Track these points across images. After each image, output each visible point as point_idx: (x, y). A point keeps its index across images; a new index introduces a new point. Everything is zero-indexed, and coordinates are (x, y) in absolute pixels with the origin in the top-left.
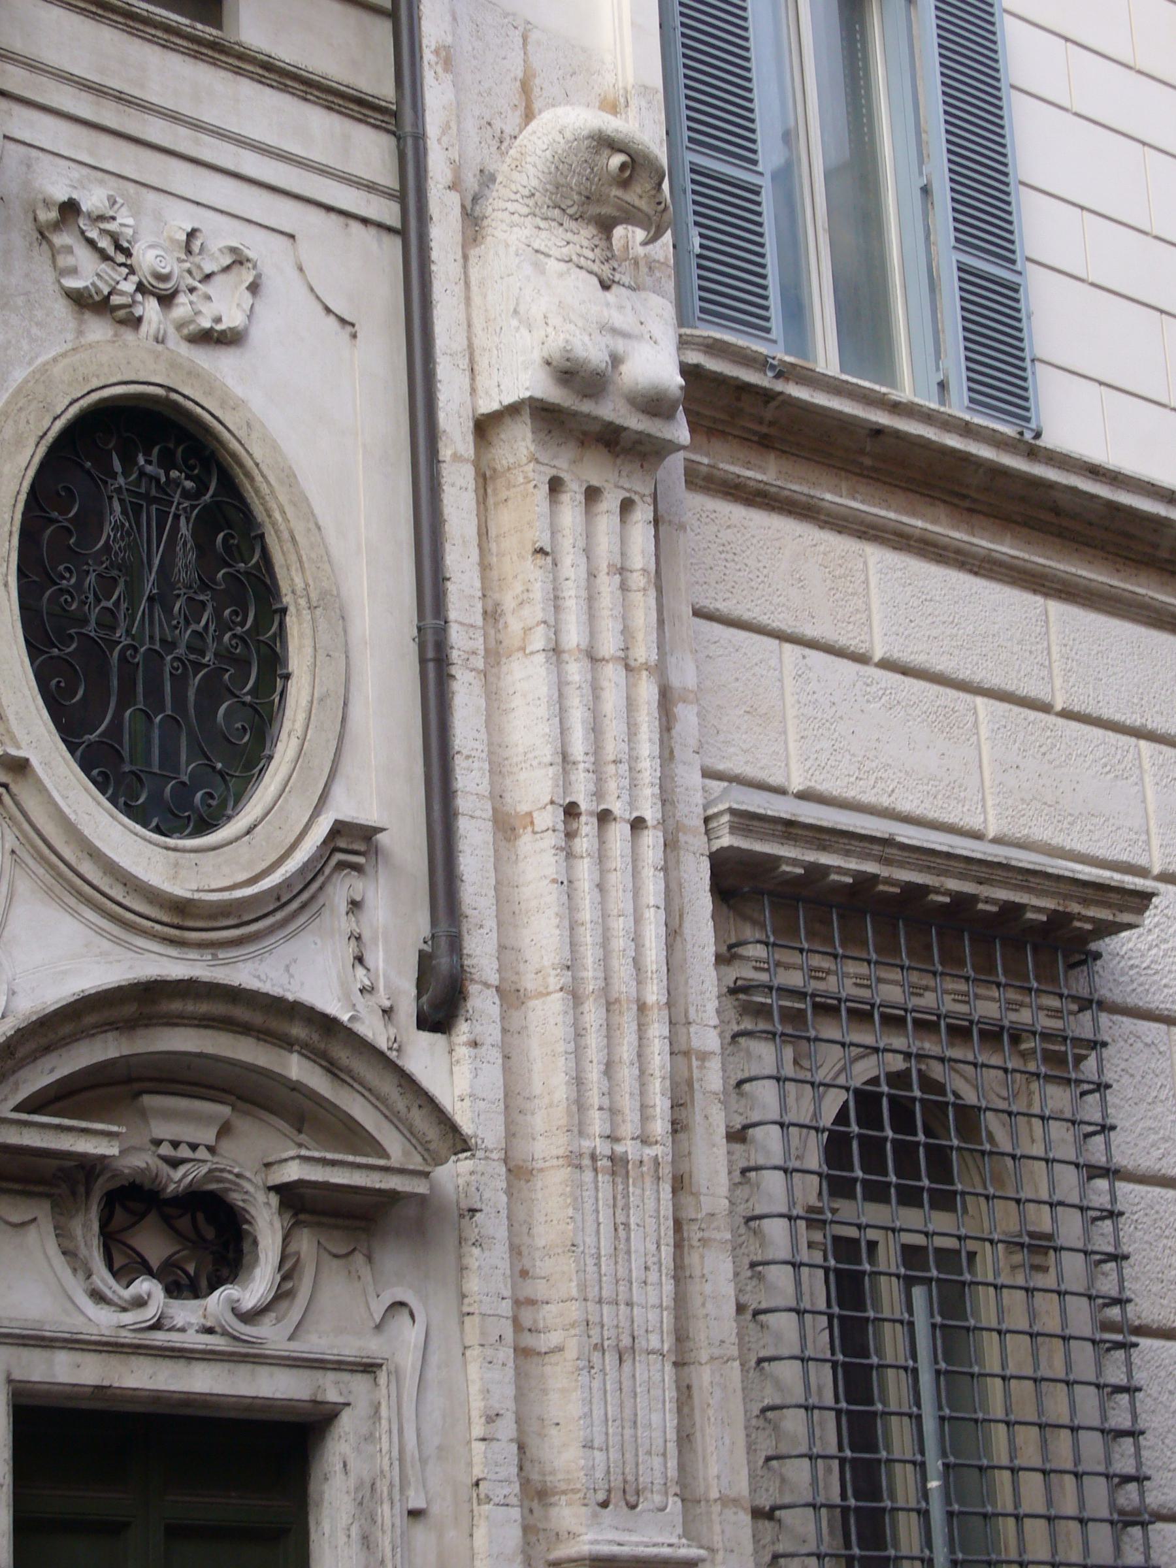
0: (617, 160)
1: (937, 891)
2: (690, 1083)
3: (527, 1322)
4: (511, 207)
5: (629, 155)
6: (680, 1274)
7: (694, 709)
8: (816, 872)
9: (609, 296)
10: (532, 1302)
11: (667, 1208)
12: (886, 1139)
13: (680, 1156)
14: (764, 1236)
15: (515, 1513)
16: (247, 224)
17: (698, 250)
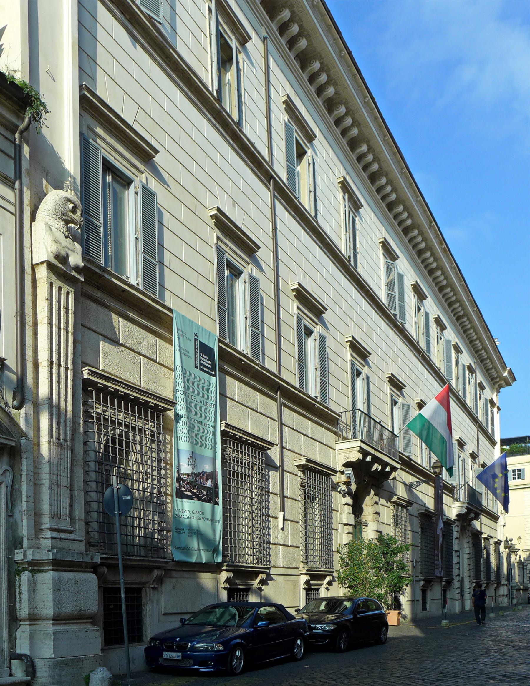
0: (71, 206)
1: (132, 395)
2: (75, 430)
3: (36, 478)
4: (44, 213)
5: (74, 204)
6: (72, 471)
7: (80, 345)
8: (106, 387)
9: (67, 239)
10: (37, 473)
11: (69, 456)
12: (123, 440)
13: (73, 446)
14: (89, 466)
15: (33, 518)
16: (6, 157)
17: (86, 238)
